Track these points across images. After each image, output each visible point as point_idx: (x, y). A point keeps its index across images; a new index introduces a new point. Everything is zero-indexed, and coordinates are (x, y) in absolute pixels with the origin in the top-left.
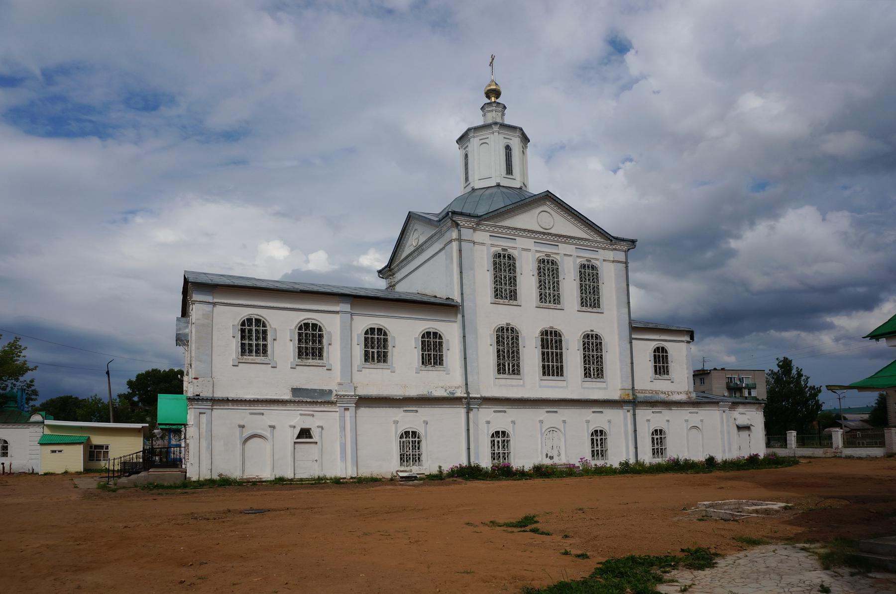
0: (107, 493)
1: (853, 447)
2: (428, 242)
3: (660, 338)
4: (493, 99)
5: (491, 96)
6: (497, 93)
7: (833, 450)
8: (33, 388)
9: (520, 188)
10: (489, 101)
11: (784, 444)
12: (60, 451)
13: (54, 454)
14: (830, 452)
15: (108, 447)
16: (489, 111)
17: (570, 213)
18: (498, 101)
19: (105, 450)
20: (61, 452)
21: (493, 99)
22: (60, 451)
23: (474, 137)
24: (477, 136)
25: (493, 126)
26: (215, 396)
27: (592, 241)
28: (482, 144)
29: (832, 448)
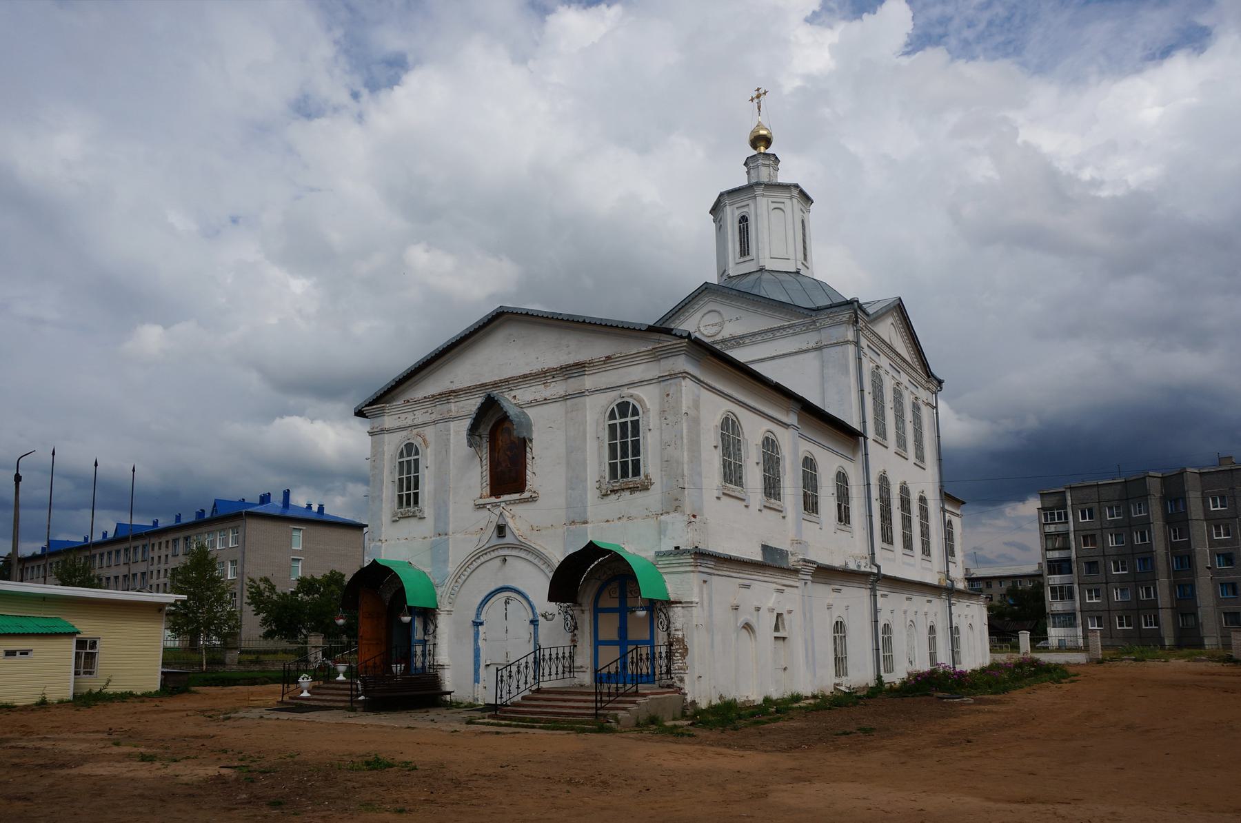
0: (415, 759)
1: (1045, 652)
2: (763, 335)
3: (873, 501)
4: (762, 149)
5: (758, 145)
6: (767, 141)
7: (1021, 655)
8: (1041, 580)
9: (798, 272)
10: (755, 152)
11: (1016, 647)
12: (25, 653)
13: (11, 660)
14: (1016, 657)
15: (95, 643)
16: (764, 165)
17: (694, 301)
18: (768, 151)
19: (88, 651)
20: (27, 654)
21: (762, 149)
22: (25, 653)
23: (763, 196)
24: (768, 196)
25: (793, 189)
26: (1212, 605)
27: (913, 369)
28: (775, 208)
29: (1019, 653)
